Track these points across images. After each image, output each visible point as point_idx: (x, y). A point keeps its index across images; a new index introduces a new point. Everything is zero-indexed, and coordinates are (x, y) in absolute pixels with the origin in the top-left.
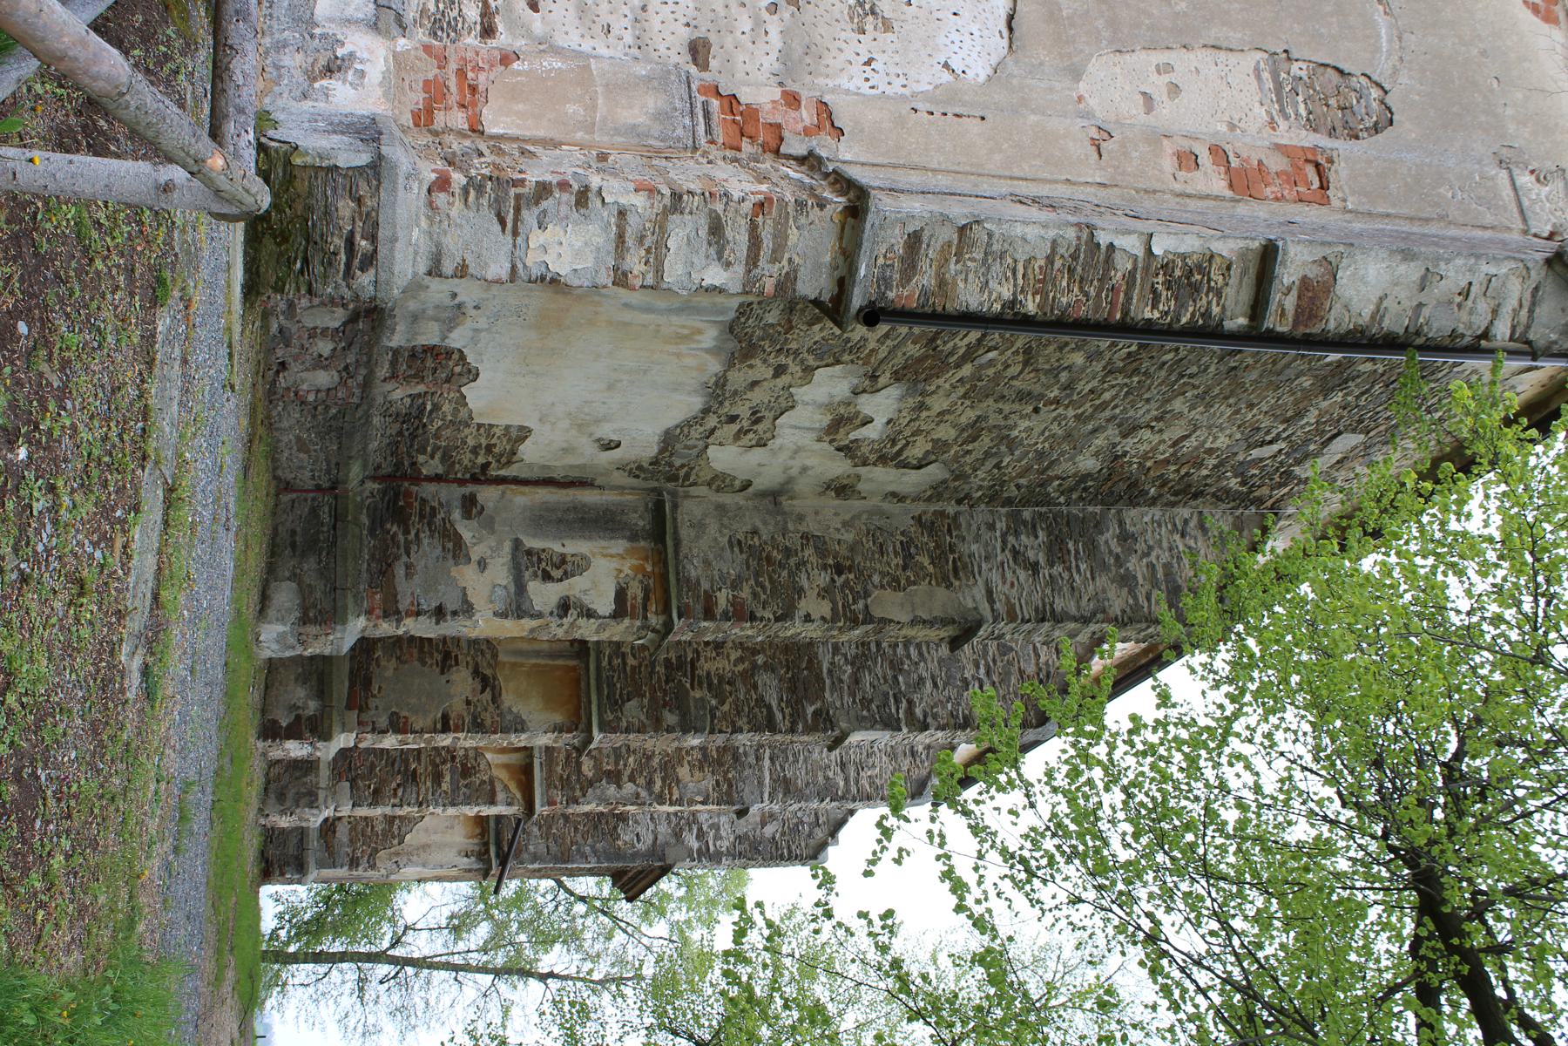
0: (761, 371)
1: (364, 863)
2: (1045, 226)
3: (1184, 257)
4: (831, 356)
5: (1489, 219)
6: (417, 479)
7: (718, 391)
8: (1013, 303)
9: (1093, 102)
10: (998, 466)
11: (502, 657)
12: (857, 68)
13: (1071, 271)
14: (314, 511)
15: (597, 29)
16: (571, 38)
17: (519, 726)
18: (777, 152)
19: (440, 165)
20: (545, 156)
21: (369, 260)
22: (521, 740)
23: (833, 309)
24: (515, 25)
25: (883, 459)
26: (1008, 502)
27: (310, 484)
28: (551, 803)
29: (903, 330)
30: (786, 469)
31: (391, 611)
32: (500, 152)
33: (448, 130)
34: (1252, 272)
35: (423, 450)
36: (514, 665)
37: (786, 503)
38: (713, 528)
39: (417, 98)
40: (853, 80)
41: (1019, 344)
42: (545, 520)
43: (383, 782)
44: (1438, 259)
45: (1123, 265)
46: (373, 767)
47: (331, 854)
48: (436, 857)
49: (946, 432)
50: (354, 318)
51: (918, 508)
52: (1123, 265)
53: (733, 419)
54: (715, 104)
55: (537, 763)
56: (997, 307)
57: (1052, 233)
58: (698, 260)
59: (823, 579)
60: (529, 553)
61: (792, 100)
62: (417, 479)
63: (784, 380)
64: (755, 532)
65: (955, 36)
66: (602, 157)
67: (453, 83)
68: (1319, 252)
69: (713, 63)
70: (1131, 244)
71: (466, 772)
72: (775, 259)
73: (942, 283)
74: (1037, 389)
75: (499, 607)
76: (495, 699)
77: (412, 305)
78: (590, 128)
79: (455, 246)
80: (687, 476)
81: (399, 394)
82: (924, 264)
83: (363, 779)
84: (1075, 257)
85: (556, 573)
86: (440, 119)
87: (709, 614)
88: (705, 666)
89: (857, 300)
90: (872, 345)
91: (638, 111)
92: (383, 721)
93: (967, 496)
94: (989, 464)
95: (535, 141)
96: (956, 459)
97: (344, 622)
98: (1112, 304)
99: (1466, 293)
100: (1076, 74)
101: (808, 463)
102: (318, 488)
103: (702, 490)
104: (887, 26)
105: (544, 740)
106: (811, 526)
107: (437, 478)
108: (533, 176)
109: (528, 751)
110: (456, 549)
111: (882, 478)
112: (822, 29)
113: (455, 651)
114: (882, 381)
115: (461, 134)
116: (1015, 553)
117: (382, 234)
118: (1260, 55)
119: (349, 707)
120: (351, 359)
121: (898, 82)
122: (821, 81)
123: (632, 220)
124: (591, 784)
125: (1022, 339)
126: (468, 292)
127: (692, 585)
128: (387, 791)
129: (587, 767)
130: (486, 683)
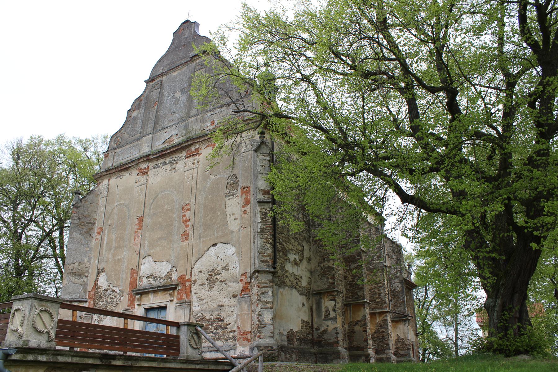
0: (287, 280)
1: (409, 347)
2: (258, 240)
3: (261, 216)
4: (283, 268)
5: (250, 157)
6: (313, 339)
7: (291, 287)
8: (271, 244)
9: (237, 229)
10: (302, 232)
11: (351, 321)
12: (235, 269)
13: (265, 235)
14: (320, 358)
15: (232, 313)
16: (234, 317)
17: (365, 316)
18: (250, 283)
19: (256, 337)
20: (254, 321)
21: (272, 347)
22: (368, 316)
23: (274, 273)
24: (233, 327)
25: (303, 254)
26: (309, 228)
27: (315, 359)
28: (386, 307)
29: (277, 257)
30: (306, 271)
31: (337, 342)
32: (254, 328)
33: (251, 336)
34: (262, 204)
35: (307, 338)
36: (353, 318)
37: (313, 270)
38: (318, 284)
39: (246, 342)
40: (237, 270)
41: (278, 236)
42: (319, 315)
43: (384, 343)
44: (257, 172)
45: (263, 226)
46: (381, 346)
47: (407, 354)
48: (406, 331)
49: (296, 244)
50: (283, 351)
51: (312, 244)
52: (263, 226)
53: (297, 283)
54: (243, 293)
55: (378, 311)
56: (271, 246)
57: (259, 239)
58: (268, 296)
59: (326, 262)
60: (325, 317)
61: (241, 280)
62: (313, 339)
63: (288, 275)
64: (319, 276)
65: (228, 253)
66: (253, 311)
67: (243, 336)
68: (258, 193)
69: (236, 294)
70: (260, 225)
71: (381, 326)
72: (267, 283)
73: (268, 256)
74: (286, 230)
75: (335, 322)
76: (359, 321)
77: (280, 341)
78: (249, 314)
79: (268, 334)
80: (309, 289)
81: (296, 343)
82: (266, 259)
83: (384, 348)
84: (262, 234)
85: (328, 312)
86: (249, 338)
87: (334, 283)
88: (350, 279)
89: (272, 270)
90: (281, 261)
91: (245, 306)
92: (365, 343)
93: (309, 236)
94: (302, 234)
95: (251, 322)
96: (301, 240)
97: (339, 351)
98: (269, 227)
99: (262, 166)
100: (232, 232)
101: (304, 267)
102: (316, 357)
103: (311, 286)
104: (227, 265)
105: (367, 311)
106: (317, 265)
107: (313, 335)
108: (257, 323)
109: (371, 314)
110: (325, 331)
111: (306, 254)
112: (229, 275)
113: (351, 330)
114: (287, 258)
115: (251, 334)
116: (319, 225)
117: (267, 346)
118: (226, 199)
119: (363, 351)
120: (290, 351)
121: (237, 263)
122: (238, 276)
123: (262, 307)
124: (381, 299)
125: (278, 235)
126: (277, 332)
127: (329, 287)
128: (386, 342)
129: (378, 300)
130: (356, 323)
